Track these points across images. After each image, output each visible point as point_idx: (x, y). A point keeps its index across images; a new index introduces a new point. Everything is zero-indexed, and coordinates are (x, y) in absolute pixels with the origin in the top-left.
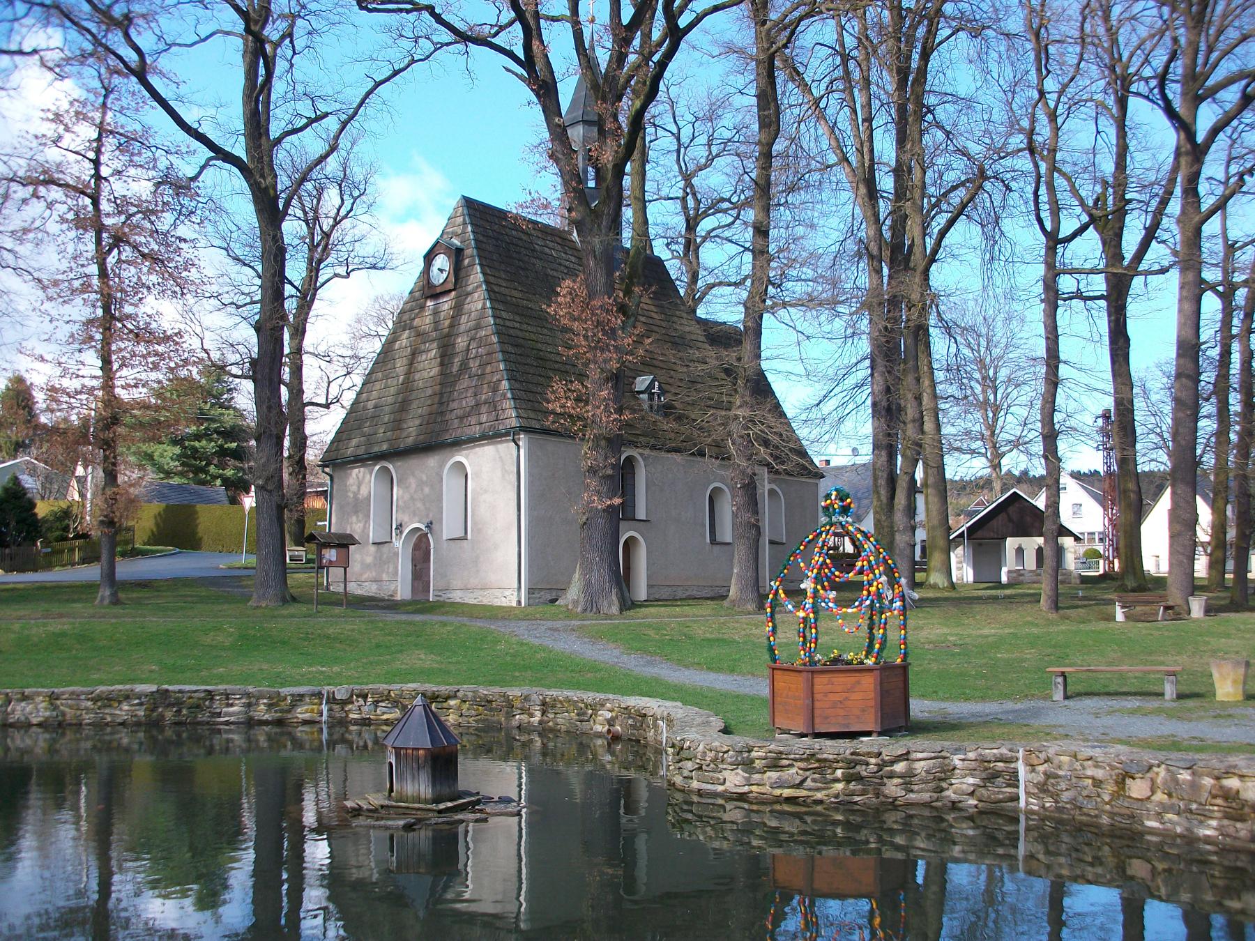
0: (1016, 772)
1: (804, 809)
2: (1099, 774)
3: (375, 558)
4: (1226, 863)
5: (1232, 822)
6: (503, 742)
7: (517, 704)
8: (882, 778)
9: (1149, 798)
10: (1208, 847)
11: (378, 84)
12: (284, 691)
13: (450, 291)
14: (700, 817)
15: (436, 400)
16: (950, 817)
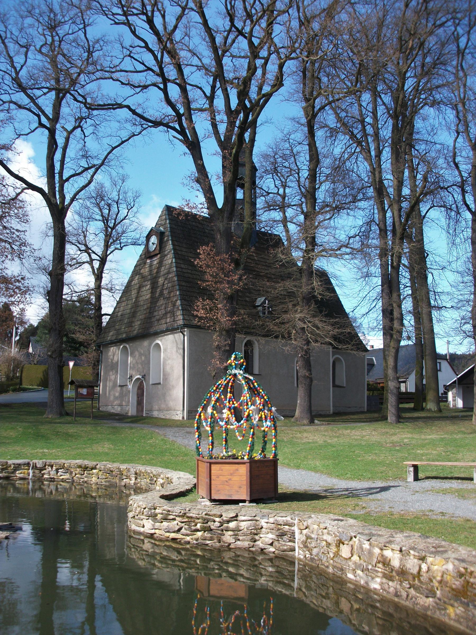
0: (293, 533)
1: (181, 547)
2: (329, 539)
3: (120, 393)
4: (385, 609)
5: (387, 581)
6: (117, 492)
7: (125, 473)
8: (222, 531)
9: (350, 558)
10: (375, 596)
11: (114, 148)
12: (10, 462)
13: (157, 254)
14: (134, 545)
15: (148, 311)
16: (260, 558)
